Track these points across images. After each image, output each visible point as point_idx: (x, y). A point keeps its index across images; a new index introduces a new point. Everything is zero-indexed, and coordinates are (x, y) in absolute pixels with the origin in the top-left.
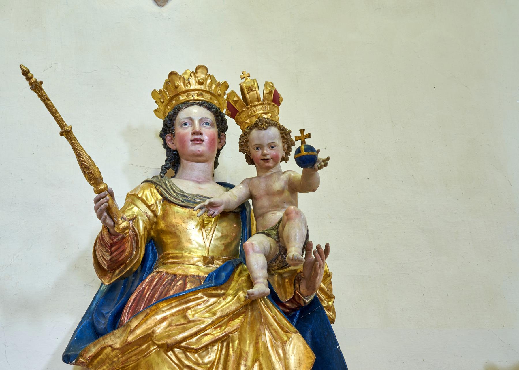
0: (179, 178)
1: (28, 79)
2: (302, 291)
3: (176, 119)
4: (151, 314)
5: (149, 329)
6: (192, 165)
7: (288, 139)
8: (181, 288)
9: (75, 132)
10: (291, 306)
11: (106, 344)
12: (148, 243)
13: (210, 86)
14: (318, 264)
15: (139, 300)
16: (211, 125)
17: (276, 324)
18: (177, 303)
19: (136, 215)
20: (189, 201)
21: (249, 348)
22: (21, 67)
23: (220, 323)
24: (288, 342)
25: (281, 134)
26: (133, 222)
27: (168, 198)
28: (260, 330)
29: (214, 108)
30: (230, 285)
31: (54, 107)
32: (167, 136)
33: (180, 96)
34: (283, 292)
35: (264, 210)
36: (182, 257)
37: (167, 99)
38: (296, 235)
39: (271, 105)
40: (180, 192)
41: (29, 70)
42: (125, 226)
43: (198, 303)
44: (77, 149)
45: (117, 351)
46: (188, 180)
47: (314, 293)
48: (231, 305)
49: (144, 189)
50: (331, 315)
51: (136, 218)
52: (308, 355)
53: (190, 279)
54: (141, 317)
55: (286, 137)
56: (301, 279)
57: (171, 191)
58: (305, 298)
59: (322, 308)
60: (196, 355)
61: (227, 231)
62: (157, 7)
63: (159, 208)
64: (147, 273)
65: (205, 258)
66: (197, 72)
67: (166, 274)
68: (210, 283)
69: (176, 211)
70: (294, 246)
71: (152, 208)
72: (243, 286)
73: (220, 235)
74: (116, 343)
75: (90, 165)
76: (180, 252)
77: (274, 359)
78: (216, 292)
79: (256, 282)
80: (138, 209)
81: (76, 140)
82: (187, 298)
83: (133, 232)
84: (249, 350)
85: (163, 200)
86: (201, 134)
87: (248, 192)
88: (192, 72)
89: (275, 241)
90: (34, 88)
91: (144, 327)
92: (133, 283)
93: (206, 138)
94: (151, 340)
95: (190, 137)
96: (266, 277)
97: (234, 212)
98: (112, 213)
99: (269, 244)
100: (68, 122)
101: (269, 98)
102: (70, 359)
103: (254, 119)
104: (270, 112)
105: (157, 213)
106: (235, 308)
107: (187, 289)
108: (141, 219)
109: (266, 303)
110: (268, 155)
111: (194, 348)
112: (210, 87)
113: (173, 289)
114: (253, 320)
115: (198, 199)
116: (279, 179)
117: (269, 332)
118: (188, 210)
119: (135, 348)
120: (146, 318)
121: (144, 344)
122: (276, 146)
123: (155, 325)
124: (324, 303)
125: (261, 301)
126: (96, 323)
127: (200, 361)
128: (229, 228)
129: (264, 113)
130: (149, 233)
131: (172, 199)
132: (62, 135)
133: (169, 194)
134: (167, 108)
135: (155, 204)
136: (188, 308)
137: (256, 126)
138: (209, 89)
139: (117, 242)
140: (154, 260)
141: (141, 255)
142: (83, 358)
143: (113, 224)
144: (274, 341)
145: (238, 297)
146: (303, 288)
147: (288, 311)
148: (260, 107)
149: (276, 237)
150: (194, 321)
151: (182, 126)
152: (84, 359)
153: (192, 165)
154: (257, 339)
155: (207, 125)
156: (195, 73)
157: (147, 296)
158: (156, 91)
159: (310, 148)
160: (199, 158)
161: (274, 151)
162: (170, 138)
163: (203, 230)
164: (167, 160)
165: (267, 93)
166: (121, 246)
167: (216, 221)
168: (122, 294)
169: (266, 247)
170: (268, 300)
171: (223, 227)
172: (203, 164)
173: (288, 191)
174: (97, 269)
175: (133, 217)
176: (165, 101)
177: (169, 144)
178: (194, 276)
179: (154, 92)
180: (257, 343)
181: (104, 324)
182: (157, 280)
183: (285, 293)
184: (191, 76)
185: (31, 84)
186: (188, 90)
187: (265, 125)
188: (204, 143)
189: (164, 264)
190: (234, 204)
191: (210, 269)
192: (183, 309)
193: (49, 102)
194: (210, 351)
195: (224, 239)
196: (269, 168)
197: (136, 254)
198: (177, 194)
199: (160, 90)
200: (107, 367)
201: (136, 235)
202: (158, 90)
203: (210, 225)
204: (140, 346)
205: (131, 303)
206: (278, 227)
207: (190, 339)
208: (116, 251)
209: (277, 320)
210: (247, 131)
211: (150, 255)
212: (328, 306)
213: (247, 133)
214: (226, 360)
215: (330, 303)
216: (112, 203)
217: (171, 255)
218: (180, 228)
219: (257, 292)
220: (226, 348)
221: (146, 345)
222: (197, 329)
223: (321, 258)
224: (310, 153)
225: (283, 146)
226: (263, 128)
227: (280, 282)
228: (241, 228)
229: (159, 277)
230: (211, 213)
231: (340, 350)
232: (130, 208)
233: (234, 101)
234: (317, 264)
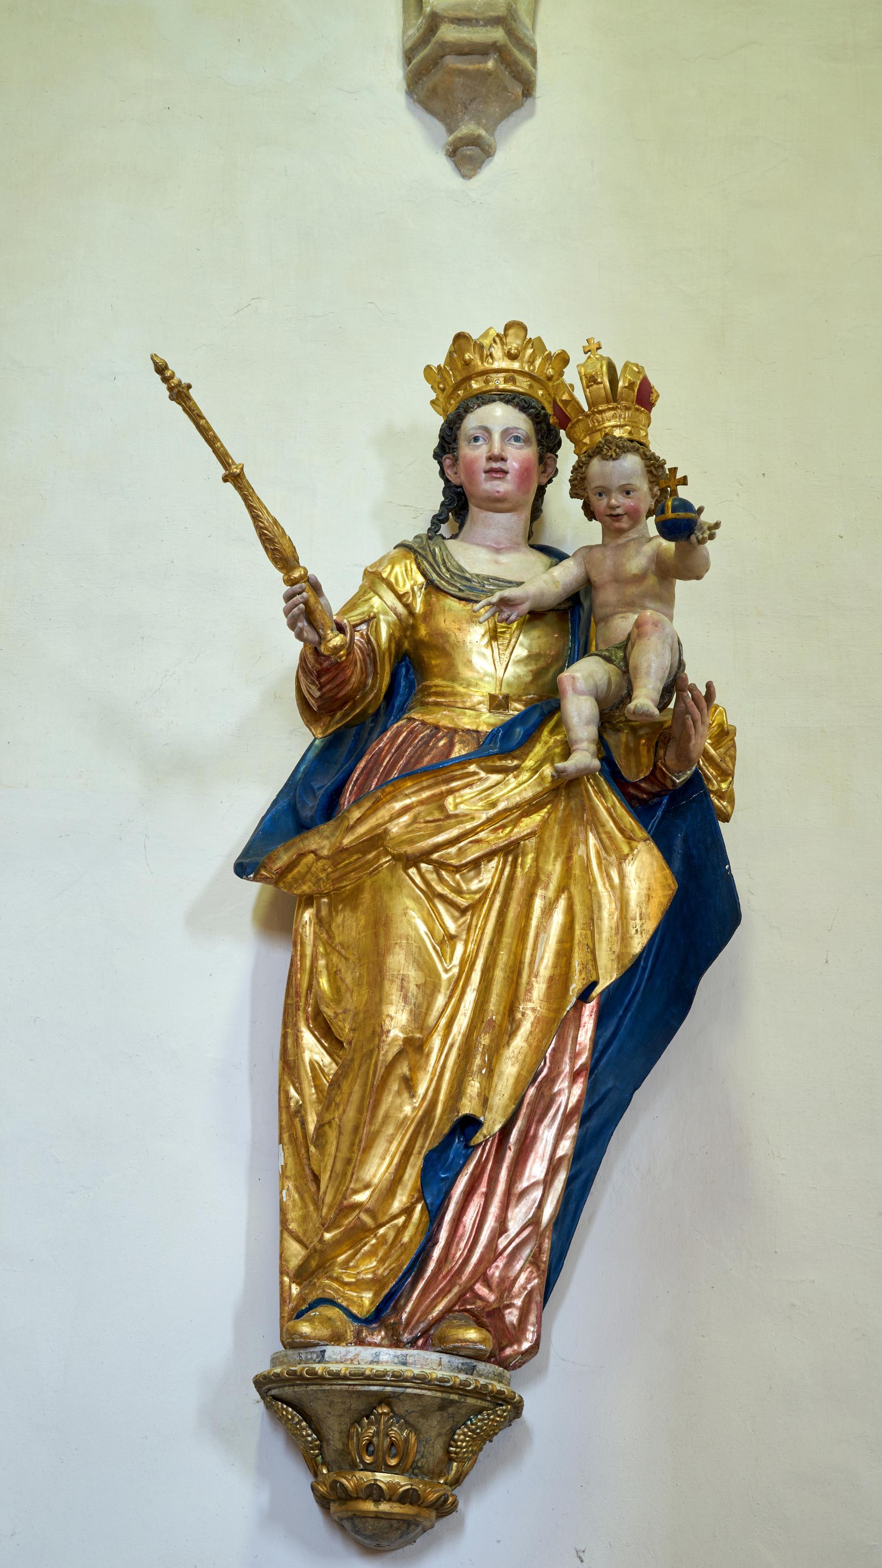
0: (462, 540)
1: (166, 380)
2: (668, 763)
3: (460, 427)
4: (384, 800)
5: (379, 826)
6: (486, 517)
7: (660, 476)
8: (443, 754)
9: (250, 475)
10: (650, 788)
11: (307, 849)
12: (400, 662)
13: (531, 360)
14: (690, 719)
15: (371, 770)
16: (524, 442)
17: (612, 824)
18: (431, 781)
19: (375, 614)
20: (472, 589)
21: (554, 869)
22: (152, 359)
23: (504, 821)
24: (630, 857)
25: (646, 466)
26: (368, 626)
27: (436, 581)
28: (577, 834)
29: (534, 407)
30: (531, 751)
31: (211, 430)
32: (445, 459)
33: (473, 382)
34: (633, 764)
35: (608, 610)
36: (454, 694)
37: (451, 384)
38: (649, 666)
39: (633, 410)
40: (458, 570)
41: (167, 364)
42: (339, 643)
43: (468, 782)
44: (252, 506)
45: (325, 861)
46: (478, 545)
47: (693, 766)
48: (525, 789)
49: (393, 562)
50: (724, 807)
51: (374, 617)
52: (665, 881)
53: (462, 736)
54: (367, 804)
55: (655, 472)
56: (670, 739)
57: (442, 567)
58: (675, 776)
59: (706, 794)
60: (458, 876)
61: (539, 646)
62: (460, 180)
63: (419, 600)
64: (395, 717)
65: (492, 697)
66: (506, 335)
67: (421, 724)
68: (491, 748)
69: (446, 608)
70: (645, 687)
71: (405, 599)
72: (554, 754)
73: (524, 653)
74: (323, 848)
75: (275, 535)
76: (449, 684)
77: (601, 888)
78: (504, 762)
79: (574, 748)
80: (380, 600)
81: (251, 490)
82: (448, 773)
83: (367, 644)
84: (554, 870)
85: (427, 584)
86: (503, 460)
87: (583, 575)
88: (498, 335)
89: (619, 671)
90: (175, 397)
91: (372, 822)
92: (370, 733)
93: (513, 465)
94: (382, 845)
95: (483, 464)
96: (594, 740)
97: (558, 610)
98: (315, 620)
99: (606, 678)
100: (237, 455)
101: (629, 395)
102: (245, 870)
103: (598, 438)
104: (630, 423)
105: (415, 609)
106: (533, 796)
107: (453, 756)
108: (385, 620)
109: (598, 784)
110: (618, 507)
111: (453, 864)
112: (531, 362)
113: (429, 753)
114: (567, 816)
115: (489, 585)
116: (638, 552)
117: (596, 839)
118: (469, 606)
119: (355, 857)
120: (376, 805)
121: (370, 852)
122: (634, 490)
123: (392, 819)
124: (713, 785)
125: (588, 780)
126: (299, 806)
127: (464, 887)
128: (544, 640)
129: (616, 426)
130: (399, 645)
131: (442, 584)
132: (225, 480)
133: (438, 575)
134: (450, 403)
135: (410, 591)
136: (451, 792)
137: (597, 451)
138: (529, 368)
139: (329, 669)
140: (410, 694)
141: (384, 686)
142: (266, 871)
143: (317, 639)
144: (603, 854)
145: (540, 775)
146: (670, 758)
147: (645, 796)
148: (609, 414)
149: (622, 663)
150: (456, 816)
151: (470, 442)
152: (269, 872)
153: (486, 517)
154: (570, 850)
155: (515, 441)
156: (501, 338)
157: (385, 764)
158: (431, 369)
159: (685, 506)
160: (500, 506)
161: (629, 500)
162: (451, 463)
163: (494, 644)
164: (443, 504)
165: (625, 387)
166: (338, 674)
167: (520, 628)
168: (351, 752)
169: (598, 684)
170: (602, 779)
171: (531, 640)
172: (508, 515)
173: (656, 575)
174: (303, 709)
175: (369, 617)
176: (447, 387)
177: (449, 473)
178: (468, 730)
179: (428, 368)
180: (569, 858)
181: (312, 808)
182: (404, 734)
183: (639, 764)
184: (495, 341)
185: (170, 389)
186: (488, 370)
187: (615, 451)
188: (509, 477)
189: (424, 704)
190: (553, 598)
191: (499, 719)
192: (442, 793)
193: (202, 422)
194: (483, 869)
195: (533, 662)
196: (621, 532)
197: (373, 685)
198: (453, 574)
199: (439, 366)
200: (310, 887)
201: (373, 650)
202: (435, 364)
203: (508, 636)
204: (365, 854)
205: (356, 775)
206: (626, 645)
207: (447, 848)
208: (328, 682)
209: (615, 815)
210: (584, 459)
211: (403, 684)
212: (720, 789)
213: (584, 464)
214: (509, 888)
215: (724, 786)
216: (315, 603)
217: (433, 690)
218: (452, 639)
219: (573, 767)
220: (511, 866)
221: (374, 853)
222: (461, 831)
223: (698, 707)
224: (682, 514)
225: (651, 489)
226: (611, 456)
227: (632, 745)
228: (568, 640)
229: (409, 729)
230: (505, 616)
231: (731, 873)
232: (367, 597)
233: (562, 401)
234: (688, 719)
